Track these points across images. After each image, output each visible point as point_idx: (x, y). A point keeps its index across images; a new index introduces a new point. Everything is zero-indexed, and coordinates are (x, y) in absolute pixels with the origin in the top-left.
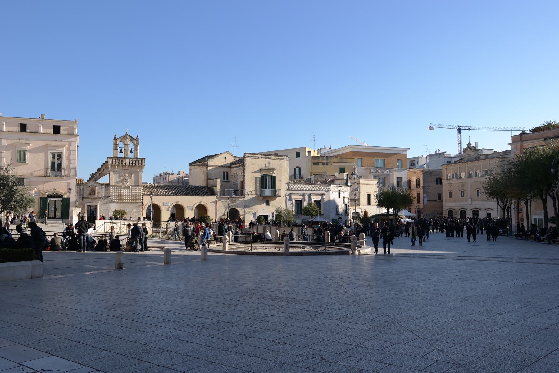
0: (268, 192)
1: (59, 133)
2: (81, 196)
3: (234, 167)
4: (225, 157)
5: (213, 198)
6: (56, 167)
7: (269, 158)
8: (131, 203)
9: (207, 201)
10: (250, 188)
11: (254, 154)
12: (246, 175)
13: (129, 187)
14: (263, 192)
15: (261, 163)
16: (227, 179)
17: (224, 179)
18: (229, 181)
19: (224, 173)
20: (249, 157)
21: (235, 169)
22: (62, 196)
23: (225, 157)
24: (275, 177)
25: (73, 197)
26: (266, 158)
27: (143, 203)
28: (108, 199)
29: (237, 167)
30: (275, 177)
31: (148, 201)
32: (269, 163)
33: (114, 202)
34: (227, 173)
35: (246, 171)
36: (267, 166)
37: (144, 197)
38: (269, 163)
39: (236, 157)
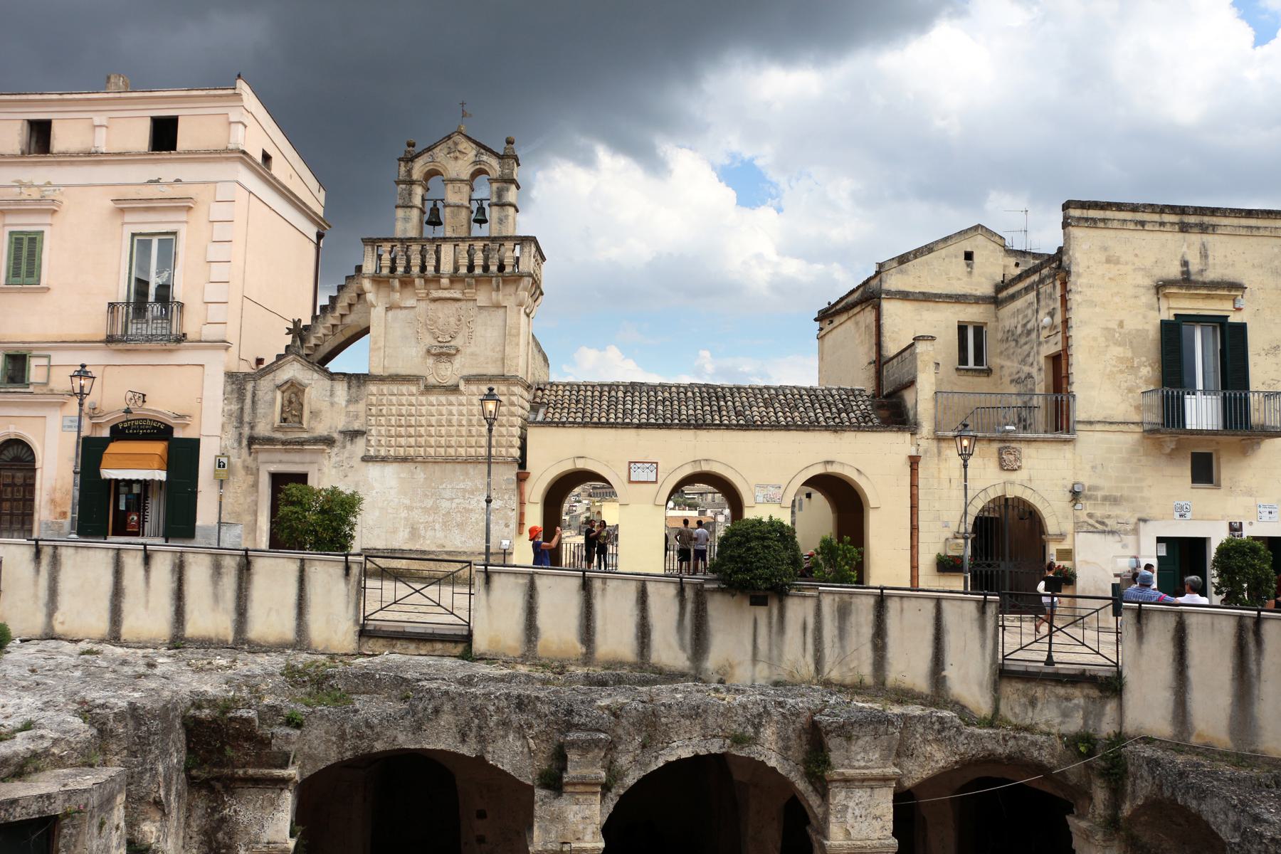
0: (1202, 411)
1: (175, 149)
2: (246, 431)
3: (1013, 298)
4: (969, 256)
5: (895, 445)
6: (151, 298)
7: (1203, 229)
8: (466, 462)
9: (871, 459)
10: (1110, 383)
11: (1119, 207)
12: (1076, 316)
13: (454, 389)
14: (1173, 413)
15: (1164, 251)
16: (979, 359)
17: (963, 359)
18: (988, 372)
19: (962, 329)
20: (1093, 223)
21: (1019, 303)
22: (169, 429)
23: (969, 256)
24: (1241, 329)
25: (213, 436)
26: (1184, 228)
27: (522, 464)
28: (359, 447)
29: (1027, 290)
30: (1241, 329)
31: (553, 452)
32: (1204, 255)
33: (384, 460)
34: (979, 330)
35: (1074, 299)
36: (1195, 266)
37: (534, 435)
38: (1204, 255)
39: (1024, 253)
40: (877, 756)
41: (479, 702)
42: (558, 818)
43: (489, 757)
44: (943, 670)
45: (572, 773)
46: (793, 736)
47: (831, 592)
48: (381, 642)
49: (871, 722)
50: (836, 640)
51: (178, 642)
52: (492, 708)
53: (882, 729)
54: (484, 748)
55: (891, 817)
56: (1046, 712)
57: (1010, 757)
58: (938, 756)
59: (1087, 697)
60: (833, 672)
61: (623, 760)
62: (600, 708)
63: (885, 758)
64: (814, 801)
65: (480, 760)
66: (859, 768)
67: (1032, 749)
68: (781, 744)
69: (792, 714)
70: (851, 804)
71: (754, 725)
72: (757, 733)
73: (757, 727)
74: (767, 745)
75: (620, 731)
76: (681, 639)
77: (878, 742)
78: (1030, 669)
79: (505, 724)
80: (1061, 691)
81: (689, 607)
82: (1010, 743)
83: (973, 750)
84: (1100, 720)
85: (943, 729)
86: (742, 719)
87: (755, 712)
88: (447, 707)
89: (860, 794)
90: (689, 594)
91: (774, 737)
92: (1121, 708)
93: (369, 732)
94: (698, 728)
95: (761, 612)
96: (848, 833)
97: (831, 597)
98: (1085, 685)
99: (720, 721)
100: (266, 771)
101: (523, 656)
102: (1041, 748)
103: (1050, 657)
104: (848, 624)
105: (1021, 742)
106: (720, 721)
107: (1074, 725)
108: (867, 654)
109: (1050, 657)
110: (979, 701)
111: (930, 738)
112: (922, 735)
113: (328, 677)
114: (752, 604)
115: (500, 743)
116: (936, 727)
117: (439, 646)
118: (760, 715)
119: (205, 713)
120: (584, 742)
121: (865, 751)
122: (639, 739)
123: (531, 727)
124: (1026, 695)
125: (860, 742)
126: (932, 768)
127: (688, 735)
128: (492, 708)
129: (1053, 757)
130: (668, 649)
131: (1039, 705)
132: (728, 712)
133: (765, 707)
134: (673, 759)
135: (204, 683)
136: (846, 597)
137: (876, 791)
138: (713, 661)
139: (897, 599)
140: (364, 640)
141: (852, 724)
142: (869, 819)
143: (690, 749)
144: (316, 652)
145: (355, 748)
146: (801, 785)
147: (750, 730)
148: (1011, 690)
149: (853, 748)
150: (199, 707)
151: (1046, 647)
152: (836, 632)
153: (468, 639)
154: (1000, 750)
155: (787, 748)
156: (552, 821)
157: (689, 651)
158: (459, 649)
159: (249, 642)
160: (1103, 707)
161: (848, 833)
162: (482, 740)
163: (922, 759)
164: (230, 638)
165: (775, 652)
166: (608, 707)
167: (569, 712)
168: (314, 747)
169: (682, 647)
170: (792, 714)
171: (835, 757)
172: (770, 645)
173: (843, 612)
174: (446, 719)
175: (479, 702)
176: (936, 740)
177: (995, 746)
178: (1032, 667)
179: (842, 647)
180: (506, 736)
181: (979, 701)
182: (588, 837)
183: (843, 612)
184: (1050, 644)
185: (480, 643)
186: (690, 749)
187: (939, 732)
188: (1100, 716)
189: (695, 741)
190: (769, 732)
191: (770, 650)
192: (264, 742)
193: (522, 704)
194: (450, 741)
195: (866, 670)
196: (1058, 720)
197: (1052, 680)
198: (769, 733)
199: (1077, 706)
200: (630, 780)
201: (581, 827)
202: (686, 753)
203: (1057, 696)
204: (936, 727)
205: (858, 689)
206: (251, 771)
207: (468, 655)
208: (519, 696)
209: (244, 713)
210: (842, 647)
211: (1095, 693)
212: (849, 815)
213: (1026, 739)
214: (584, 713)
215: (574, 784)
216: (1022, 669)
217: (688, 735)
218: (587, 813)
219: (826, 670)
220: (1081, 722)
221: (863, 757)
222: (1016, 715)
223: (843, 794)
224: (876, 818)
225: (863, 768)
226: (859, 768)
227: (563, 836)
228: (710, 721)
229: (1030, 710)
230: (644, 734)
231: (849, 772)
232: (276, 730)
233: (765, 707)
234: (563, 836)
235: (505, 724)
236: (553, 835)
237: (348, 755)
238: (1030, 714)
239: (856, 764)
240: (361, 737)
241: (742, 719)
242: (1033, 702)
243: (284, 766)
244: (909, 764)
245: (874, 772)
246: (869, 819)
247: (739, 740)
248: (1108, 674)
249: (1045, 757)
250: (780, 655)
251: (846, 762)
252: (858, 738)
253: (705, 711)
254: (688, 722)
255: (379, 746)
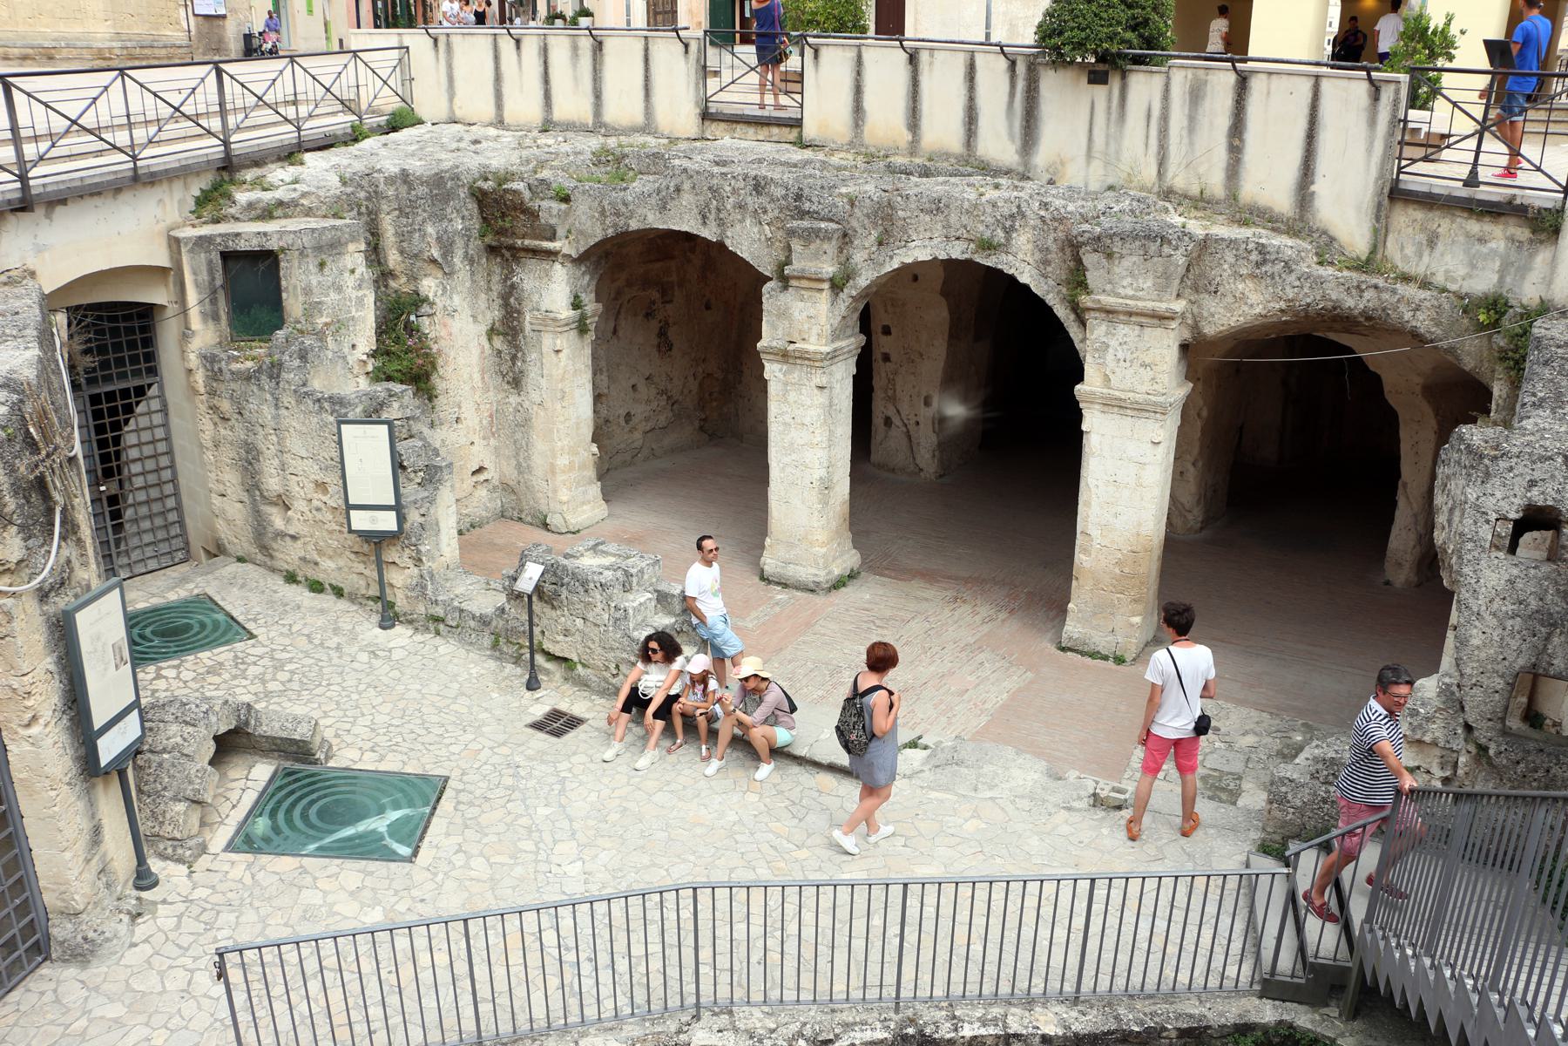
40: (1149, 283)
41: (715, 181)
42: (784, 314)
43: (728, 242)
44: (1313, 183)
45: (797, 265)
46: (1054, 247)
47: (1182, 67)
48: (723, 125)
49: (1136, 237)
50: (1185, 133)
51: (547, 126)
52: (728, 189)
53: (1153, 247)
54: (723, 232)
55: (1402, 445)
56: (1448, 258)
57: (1364, 313)
58: (1254, 298)
59: (1512, 239)
60: (1179, 178)
61: (858, 257)
62: (841, 195)
63: (1162, 289)
64: (1074, 331)
65: (721, 245)
66: (1126, 297)
67: (1402, 308)
68: (1038, 256)
69: (1054, 219)
70: (1113, 343)
71: (1004, 228)
72: (1009, 239)
73: (1008, 231)
74: (1020, 256)
75: (855, 223)
76: (1011, 126)
77: (1149, 264)
78: (1436, 191)
79: (741, 206)
80: (1474, 226)
81: (1021, 85)
82: (1367, 295)
83: (1308, 297)
84: (1523, 278)
85: (1265, 262)
86: (990, 220)
87: (1006, 212)
88: (687, 186)
89: (1125, 331)
90: (1021, 68)
91: (1030, 246)
92: (1553, 264)
93: (623, 209)
94: (939, 226)
95: (1100, 91)
96: (1107, 379)
97: (1182, 73)
98: (1512, 221)
99: (965, 219)
100: (537, 243)
101: (851, 143)
102: (1417, 309)
103: (1474, 172)
104: (1200, 111)
105: (1385, 296)
106: (965, 219)
107: (1483, 283)
108: (1221, 155)
109: (1474, 172)
110: (1354, 233)
111: (1244, 271)
112: (1231, 266)
113: (625, 156)
114: (1090, 82)
115: (738, 227)
116: (1254, 257)
117: (775, 130)
118: (1012, 216)
119: (488, 185)
120: (805, 230)
121: (1132, 274)
122: (875, 234)
123: (765, 212)
124: (1423, 229)
125: (1126, 263)
126: (1244, 314)
127: (928, 234)
128: (728, 189)
129: (1438, 324)
130: (997, 143)
131: (1440, 247)
132: (973, 210)
133: (1019, 207)
134: (909, 260)
135: (500, 155)
136: (1201, 73)
137: (1148, 331)
138: (1043, 156)
139: (1263, 76)
140: (707, 123)
141: (1111, 237)
142: (1136, 365)
143: (929, 251)
144: (662, 137)
145: (615, 225)
146: (1061, 312)
147: (1000, 233)
148: (1406, 220)
149: (1117, 270)
150: (486, 179)
151: (1470, 157)
152: (1185, 123)
153: (797, 123)
154: (1350, 302)
155: (1046, 262)
156: (779, 316)
157: (1018, 142)
158: (793, 135)
159: (605, 125)
160: (1531, 256)
161: (1107, 379)
162: (721, 223)
163: (1230, 299)
164: (590, 122)
165: (1113, 147)
166: (847, 195)
167: (798, 197)
168: (584, 225)
169: (1011, 136)
170: (1054, 219)
171: (1093, 278)
172: (1108, 136)
173: (1196, 95)
174: (687, 199)
175: (715, 181)
176: (1253, 276)
177: (1344, 296)
178: (1439, 187)
179: (1191, 143)
180: (742, 221)
181: (1354, 233)
182: (813, 339)
183: (1196, 95)
184: (1478, 152)
185: (810, 130)
186: (929, 251)
187: (1258, 265)
188: (1524, 270)
189: (935, 241)
190: (1023, 239)
191: (1107, 144)
192: (533, 215)
193: (759, 186)
194: (692, 223)
195: (1216, 183)
196: (1462, 271)
197: (1464, 209)
198: (1023, 241)
199: (1494, 252)
200: (863, 281)
201: (806, 326)
202: (924, 255)
203: (1468, 235)
204: (1254, 257)
205: (1200, 203)
206: (527, 242)
207: (801, 144)
208: (755, 178)
209: (515, 185)
210: (1191, 143)
211: (1523, 233)
212: (1110, 357)
213: (1394, 292)
214: (815, 199)
215: (799, 278)
216: (1425, 189)
217: (928, 234)
218: (812, 312)
219: (1170, 174)
220: (1495, 278)
221: (1123, 282)
222: (1405, 258)
223: (1103, 328)
224: (1144, 365)
225: (1131, 298)
226: (1126, 297)
227: (789, 334)
228: (953, 219)
229: (1426, 253)
230: (881, 229)
231: (1108, 300)
232: (545, 204)
233: (1019, 207)
234: (789, 334)
235: (741, 206)
236: (780, 332)
237: (610, 232)
238: (1426, 259)
239: (1121, 291)
240: (617, 214)
241: (990, 220)
242: (1432, 242)
243: (552, 238)
244: (1210, 305)
245: (1140, 304)
246: (1136, 365)
247: (987, 246)
248: (1549, 205)
249: (1422, 322)
250: (1118, 152)
251: (1108, 287)
252: (1122, 257)
253: (947, 206)
254: (927, 218)
255: (634, 225)
